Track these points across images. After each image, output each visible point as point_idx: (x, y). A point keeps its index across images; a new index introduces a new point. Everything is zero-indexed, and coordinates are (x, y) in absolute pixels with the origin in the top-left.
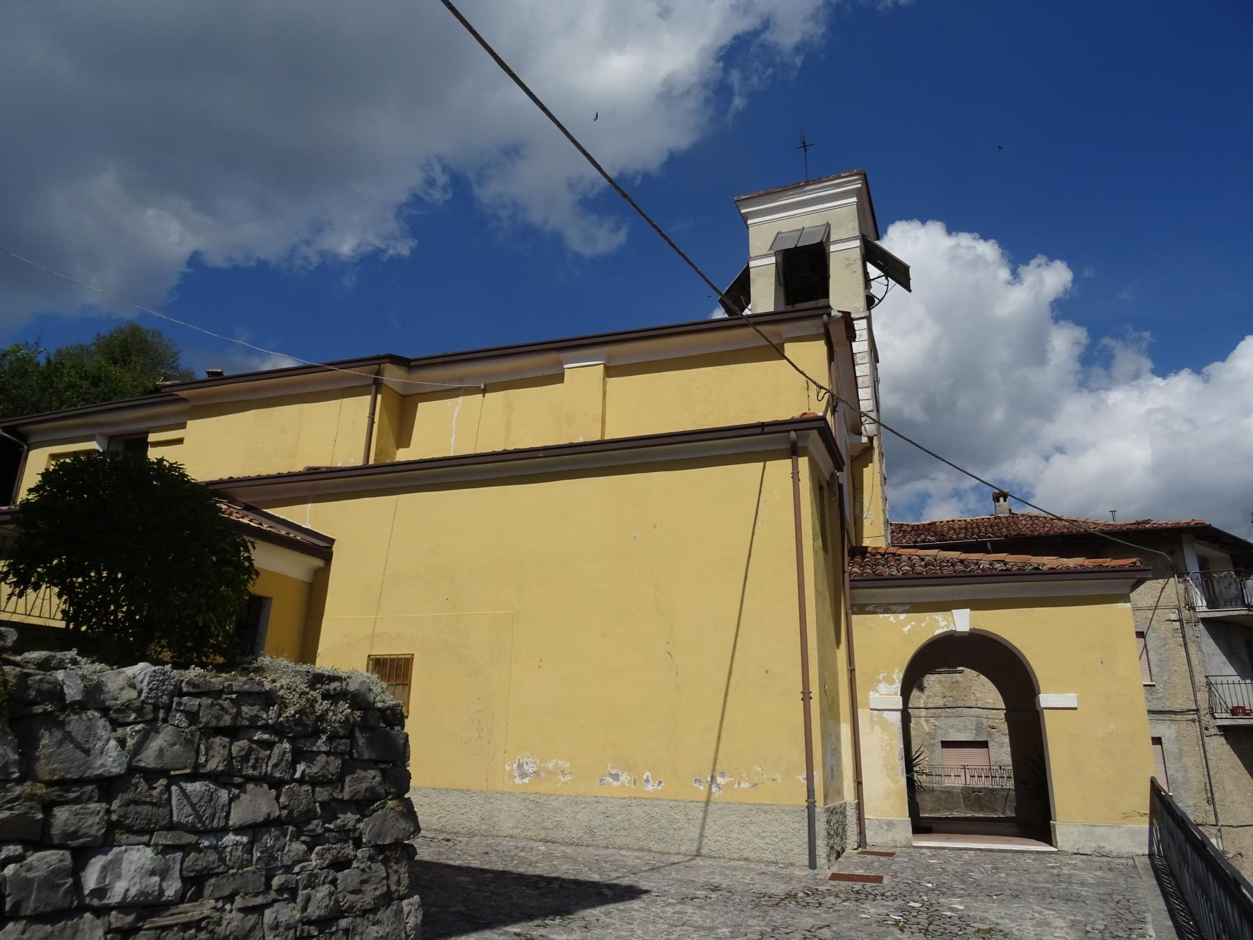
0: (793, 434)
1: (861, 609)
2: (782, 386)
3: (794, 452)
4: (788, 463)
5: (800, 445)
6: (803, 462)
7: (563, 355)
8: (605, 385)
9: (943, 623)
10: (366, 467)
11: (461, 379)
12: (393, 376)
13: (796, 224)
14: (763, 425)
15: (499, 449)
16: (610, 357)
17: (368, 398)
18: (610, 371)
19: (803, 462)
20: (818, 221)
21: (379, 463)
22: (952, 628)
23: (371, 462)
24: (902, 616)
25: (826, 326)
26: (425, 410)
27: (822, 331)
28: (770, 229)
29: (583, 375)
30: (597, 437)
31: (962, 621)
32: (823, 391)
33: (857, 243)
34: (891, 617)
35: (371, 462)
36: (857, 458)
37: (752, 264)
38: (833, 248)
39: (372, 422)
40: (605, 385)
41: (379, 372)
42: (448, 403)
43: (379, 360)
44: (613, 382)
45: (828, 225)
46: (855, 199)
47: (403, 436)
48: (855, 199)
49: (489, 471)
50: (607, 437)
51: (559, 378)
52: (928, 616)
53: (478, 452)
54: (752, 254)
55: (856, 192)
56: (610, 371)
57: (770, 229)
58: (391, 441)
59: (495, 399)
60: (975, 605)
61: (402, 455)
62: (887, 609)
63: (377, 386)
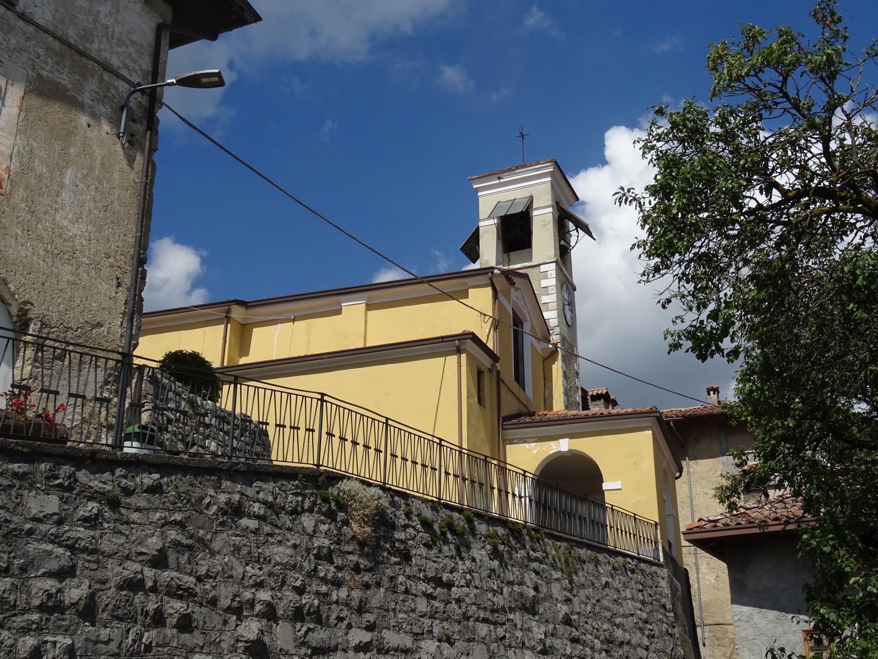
0: (457, 342)
1: (512, 442)
2: (472, 313)
3: (458, 351)
4: (455, 357)
5: (461, 347)
6: (464, 356)
7: (341, 298)
8: (366, 315)
9: (554, 447)
10: (223, 368)
11: (279, 313)
12: (237, 313)
13: (510, 196)
14: (443, 337)
15: (302, 354)
16: (369, 299)
17: (222, 327)
18: (369, 307)
19: (464, 356)
20: (525, 194)
21: (231, 365)
22: (559, 449)
23: (225, 364)
24: (533, 444)
25: (491, 279)
26: (256, 332)
27: (489, 282)
28: (493, 198)
29: (353, 310)
30: (362, 346)
31: (564, 445)
32: (487, 318)
33: (550, 210)
34: (527, 445)
35: (225, 364)
36: (547, 358)
37: (481, 224)
38: (535, 213)
39: (225, 342)
40: (366, 315)
41: (229, 311)
42: (271, 328)
43: (229, 303)
44: (372, 314)
45: (531, 200)
46: (549, 179)
47: (244, 349)
48: (549, 179)
49: (298, 367)
50: (368, 345)
51: (339, 312)
52: (546, 444)
53: (291, 356)
54: (481, 217)
55: (551, 174)
56: (369, 307)
57: (493, 198)
58: (237, 353)
59: (300, 324)
60: (572, 436)
61: (243, 361)
62: (524, 441)
63: (228, 319)
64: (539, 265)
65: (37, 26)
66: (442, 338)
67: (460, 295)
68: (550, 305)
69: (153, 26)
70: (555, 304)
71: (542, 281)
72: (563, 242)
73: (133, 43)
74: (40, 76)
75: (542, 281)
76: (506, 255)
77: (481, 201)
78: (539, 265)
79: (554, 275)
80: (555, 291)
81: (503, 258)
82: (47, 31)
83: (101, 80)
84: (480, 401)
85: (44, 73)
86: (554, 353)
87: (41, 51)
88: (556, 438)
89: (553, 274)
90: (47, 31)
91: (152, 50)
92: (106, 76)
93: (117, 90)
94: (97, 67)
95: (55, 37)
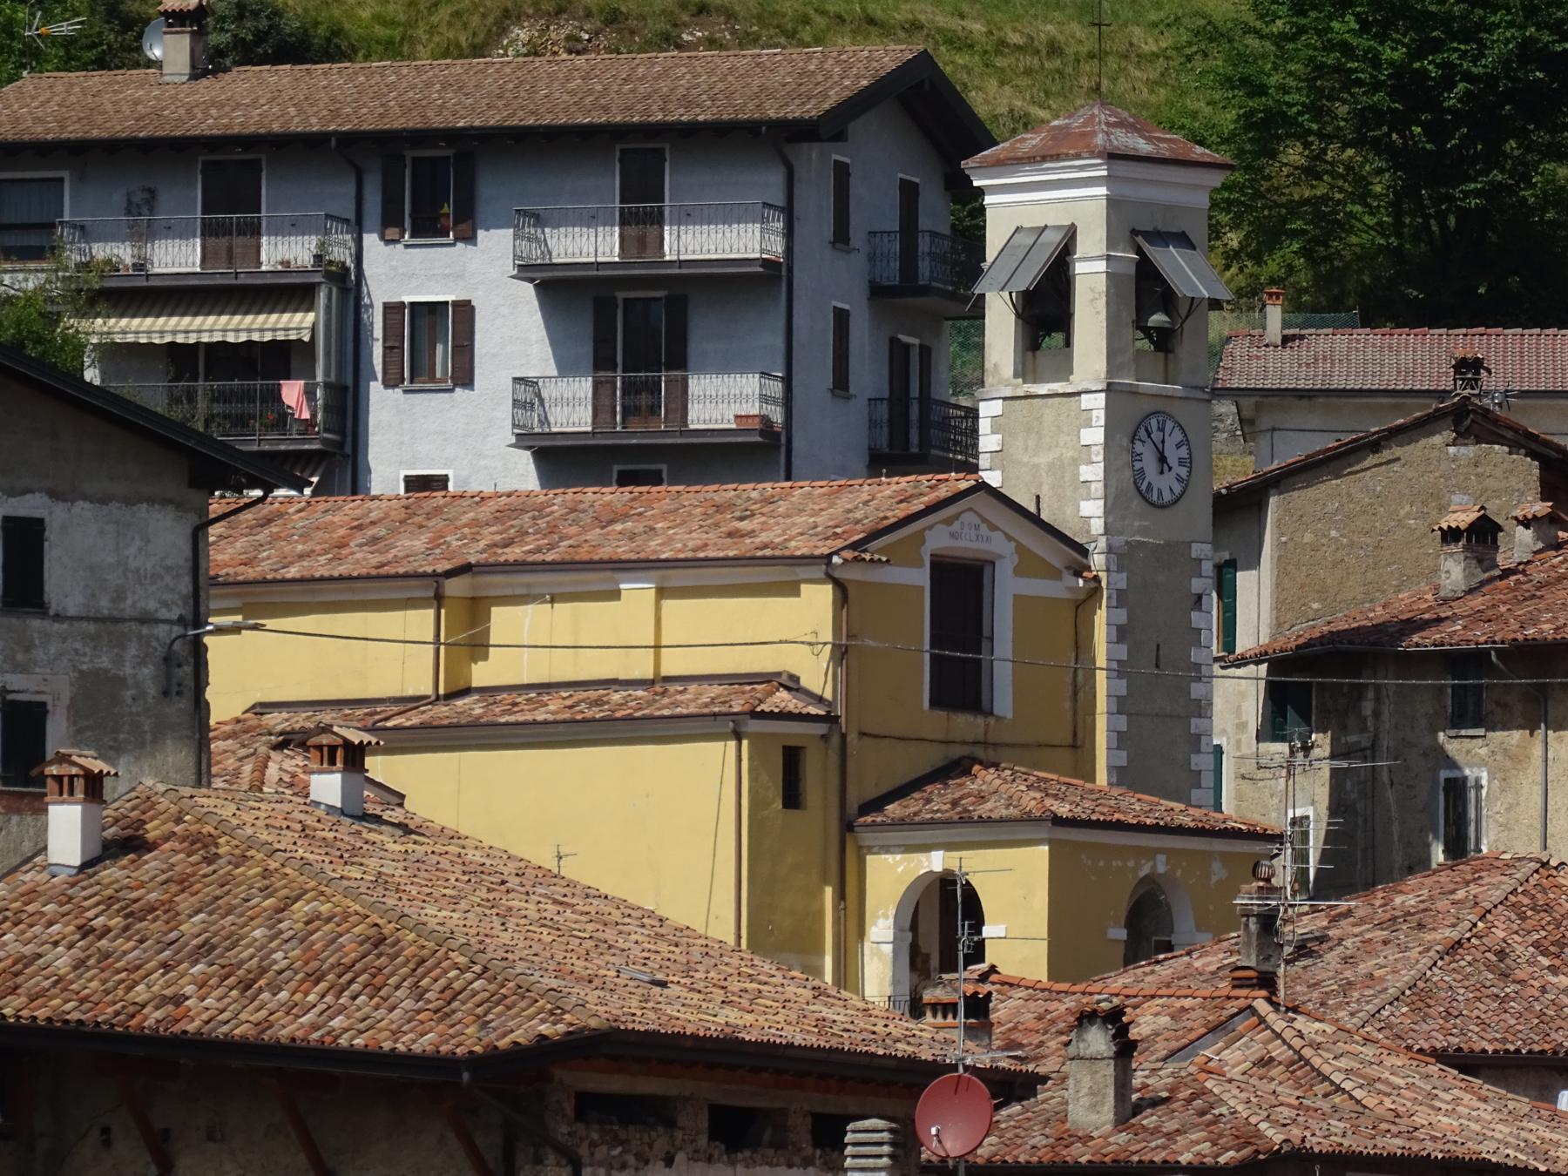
17: (431, 612)
18: (662, 593)
24: (898, 857)
34: (889, 858)
35: (441, 692)
44: (669, 605)
51: (615, 595)
60: (949, 847)
62: (886, 849)
64: (1079, 394)
65: (72, 618)
66: (1137, 298)
67: (792, 589)
68: (1093, 486)
69: (189, 531)
70: (1101, 486)
71: (1083, 432)
72: (1158, 319)
73: (168, 569)
74: (81, 672)
75: (1083, 432)
76: (1029, 354)
77: (990, 214)
78: (1079, 394)
79: (1102, 422)
80: (1101, 458)
81: (1024, 364)
82: (81, 619)
83: (140, 637)
84: (792, 798)
85: (84, 667)
86: (1094, 592)
87: (78, 645)
88: (926, 848)
89: (1099, 417)
90: (81, 619)
91: (190, 564)
92: (145, 630)
93: (157, 639)
94: (134, 626)
95: (87, 619)
